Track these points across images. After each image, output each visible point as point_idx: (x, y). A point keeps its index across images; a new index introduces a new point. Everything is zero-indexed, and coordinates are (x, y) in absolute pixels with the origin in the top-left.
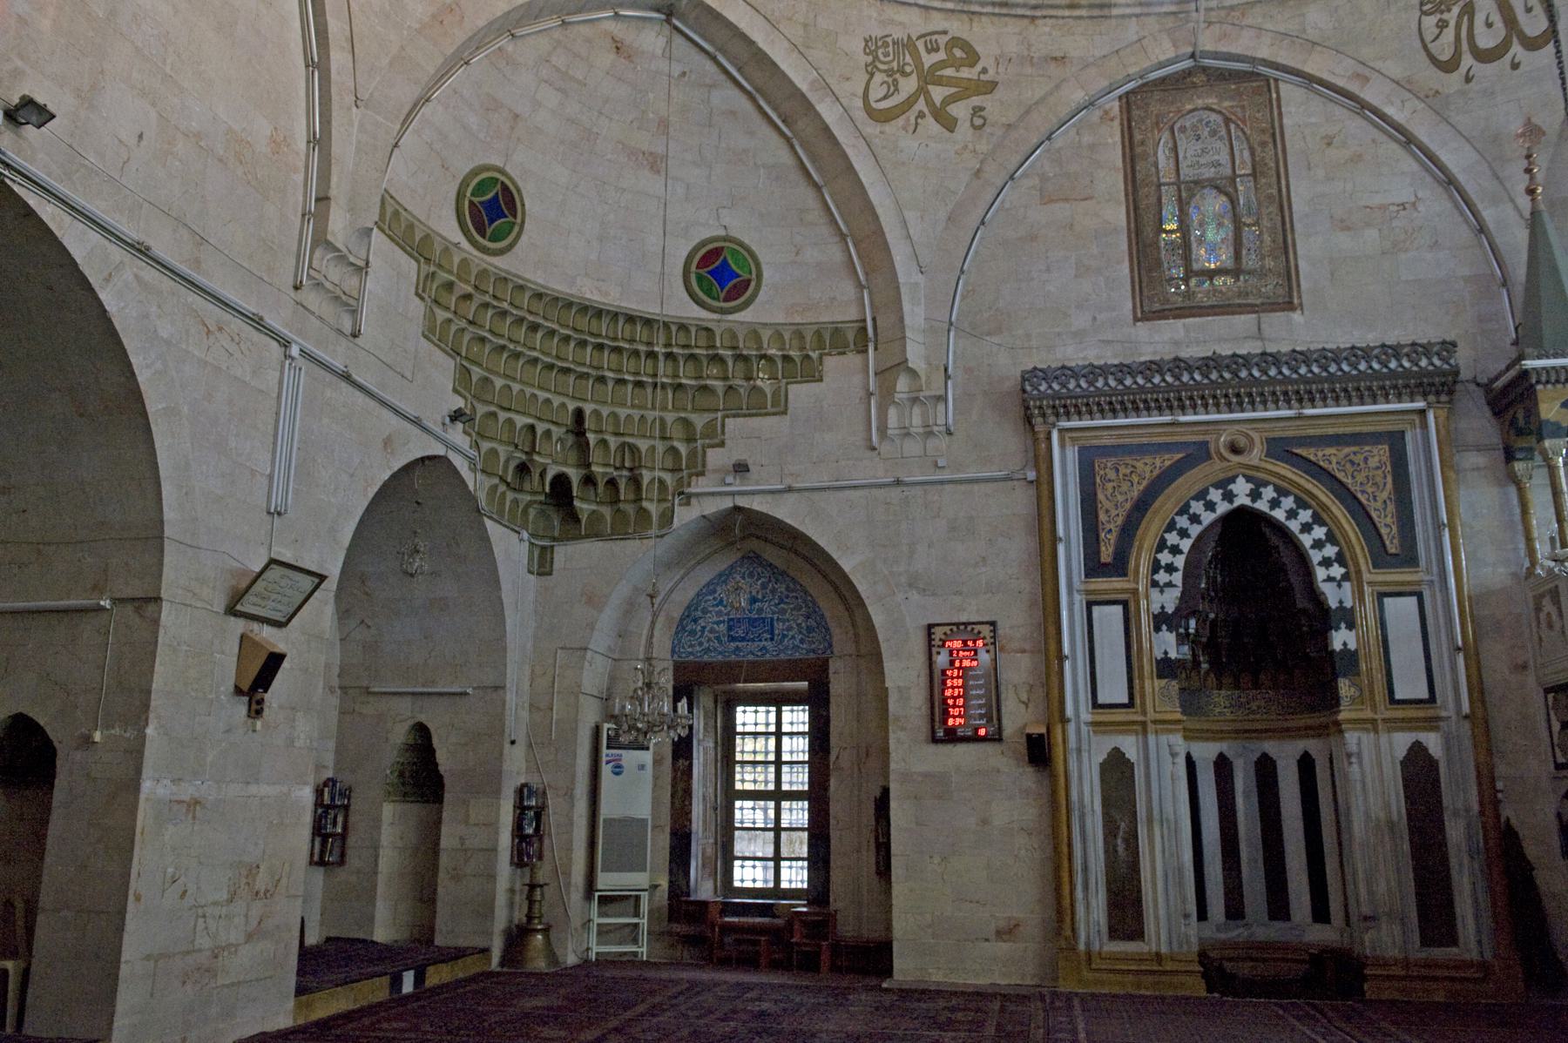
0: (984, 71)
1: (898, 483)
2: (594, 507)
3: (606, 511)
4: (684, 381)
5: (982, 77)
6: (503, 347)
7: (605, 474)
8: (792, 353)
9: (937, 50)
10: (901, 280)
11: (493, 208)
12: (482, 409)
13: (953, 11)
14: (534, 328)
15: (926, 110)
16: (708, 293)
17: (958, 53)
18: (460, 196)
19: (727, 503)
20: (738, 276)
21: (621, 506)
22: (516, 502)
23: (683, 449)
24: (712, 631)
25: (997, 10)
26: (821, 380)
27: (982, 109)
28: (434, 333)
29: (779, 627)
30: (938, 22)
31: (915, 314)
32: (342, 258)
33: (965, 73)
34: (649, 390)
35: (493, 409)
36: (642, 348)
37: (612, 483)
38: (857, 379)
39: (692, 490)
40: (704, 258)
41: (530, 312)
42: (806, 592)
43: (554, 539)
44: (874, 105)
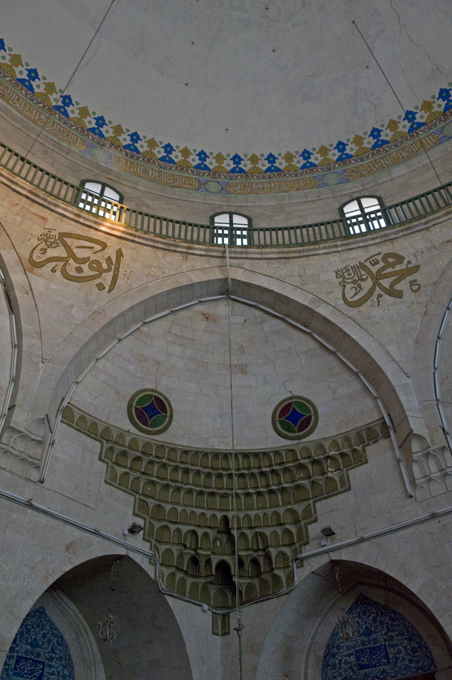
0: (409, 262)
1: (434, 516)
2: (248, 581)
3: (256, 582)
4: (285, 485)
5: (409, 266)
6: (167, 486)
7: (247, 556)
8: (344, 450)
9: (378, 262)
10: (394, 383)
11: (151, 409)
12: (157, 525)
13: (381, 243)
14: (187, 471)
15: (382, 293)
16: (289, 429)
17: (391, 260)
18: (130, 406)
19: (325, 559)
20: (304, 415)
21: (263, 576)
22: (194, 585)
23: (293, 529)
24: (346, 663)
25: (405, 233)
26: (367, 462)
27: (415, 281)
28: (111, 480)
29: (391, 651)
30: (374, 250)
31: (410, 402)
32: (24, 437)
33: (398, 268)
34: (267, 496)
35: (164, 523)
36: (256, 471)
37: (255, 561)
38: (389, 455)
39: (303, 555)
40: (281, 412)
41: (182, 463)
42: (404, 619)
43: (229, 608)
44: (350, 300)
